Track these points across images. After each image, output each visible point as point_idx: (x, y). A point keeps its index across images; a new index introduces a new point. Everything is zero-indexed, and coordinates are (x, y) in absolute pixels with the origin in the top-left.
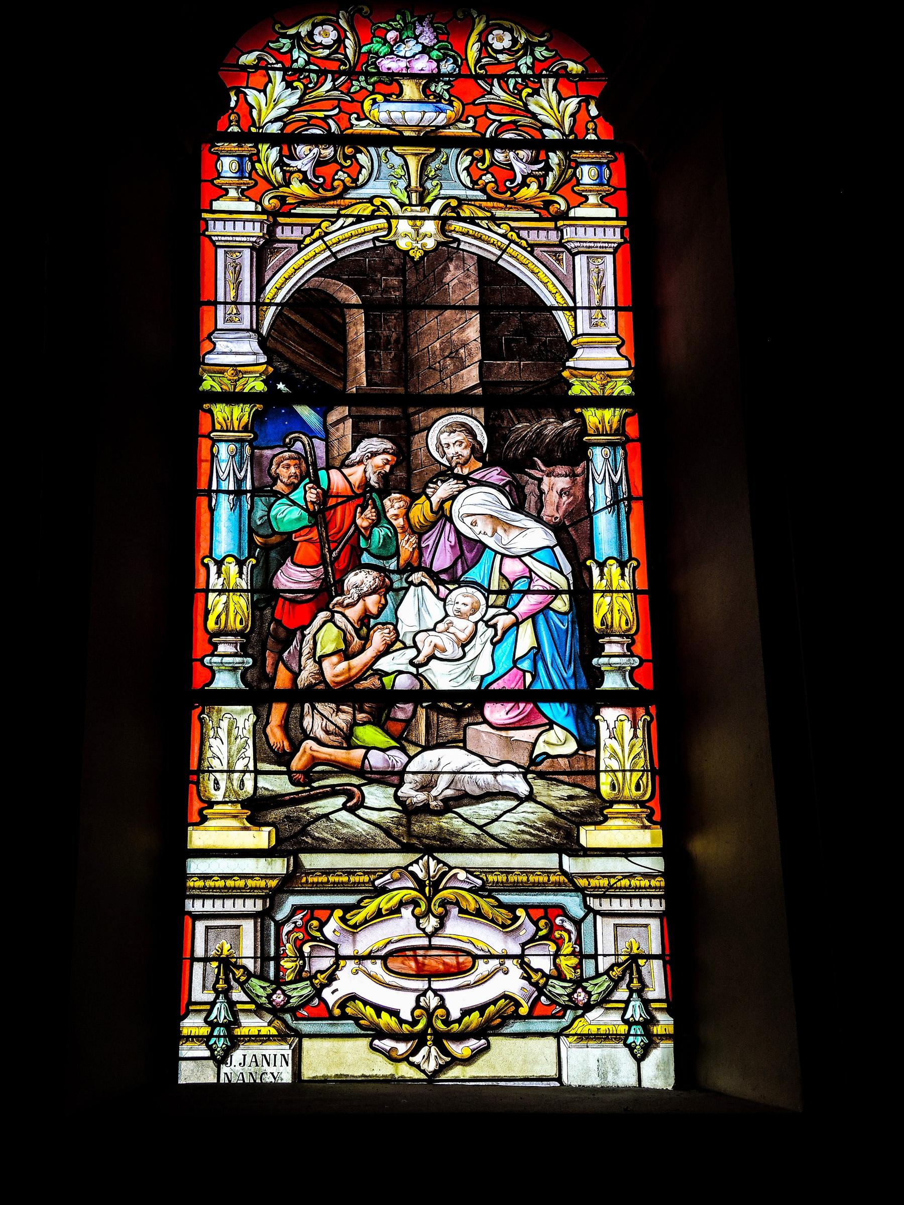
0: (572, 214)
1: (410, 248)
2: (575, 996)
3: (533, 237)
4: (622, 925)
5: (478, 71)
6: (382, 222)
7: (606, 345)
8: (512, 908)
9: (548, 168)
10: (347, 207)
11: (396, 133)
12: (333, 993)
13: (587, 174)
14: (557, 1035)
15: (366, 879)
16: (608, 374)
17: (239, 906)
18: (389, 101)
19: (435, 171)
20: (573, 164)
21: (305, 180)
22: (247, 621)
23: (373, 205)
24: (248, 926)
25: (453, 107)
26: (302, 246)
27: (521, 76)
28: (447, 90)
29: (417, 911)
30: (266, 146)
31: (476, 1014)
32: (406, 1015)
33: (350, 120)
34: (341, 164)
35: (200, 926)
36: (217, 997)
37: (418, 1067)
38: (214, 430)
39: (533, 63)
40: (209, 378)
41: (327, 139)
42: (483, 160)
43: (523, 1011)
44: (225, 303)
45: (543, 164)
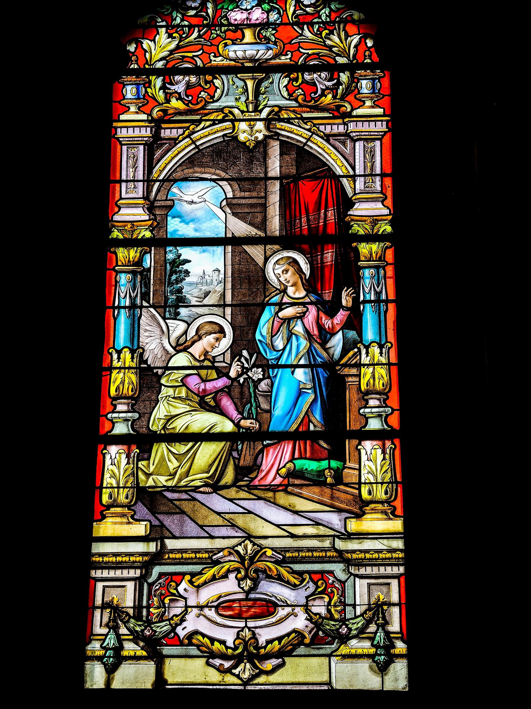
0: (354, 113)
1: (247, 140)
2: (340, 630)
3: (328, 130)
4: (108, 587)
5: (294, 19)
6: (228, 124)
7: (136, 206)
8: (301, 573)
9: (339, 83)
10: (206, 115)
11: (240, 65)
12: (183, 629)
13: (365, 86)
14: (330, 656)
15: (206, 555)
16: (375, 220)
17: (389, 570)
18: (235, 44)
19: (265, 88)
20: (356, 80)
21: (179, 98)
22: (136, 390)
23: (223, 113)
24: (130, 586)
25: (277, 46)
26: (177, 142)
27: (322, 22)
28: (273, 35)
29: (239, 576)
30: (154, 77)
31: (276, 642)
32: (230, 644)
33: (210, 57)
34: (203, 87)
35: (100, 586)
36: (378, 629)
37: (238, 676)
38: (117, 265)
39: (330, 13)
40: (116, 230)
41: (196, 71)
42: (296, 80)
43: (307, 641)
44: (127, 181)
45: (336, 80)
